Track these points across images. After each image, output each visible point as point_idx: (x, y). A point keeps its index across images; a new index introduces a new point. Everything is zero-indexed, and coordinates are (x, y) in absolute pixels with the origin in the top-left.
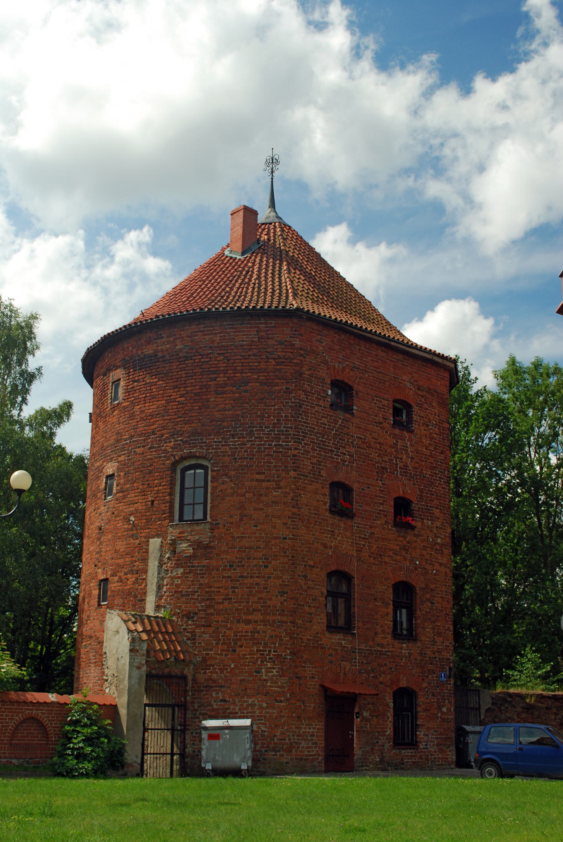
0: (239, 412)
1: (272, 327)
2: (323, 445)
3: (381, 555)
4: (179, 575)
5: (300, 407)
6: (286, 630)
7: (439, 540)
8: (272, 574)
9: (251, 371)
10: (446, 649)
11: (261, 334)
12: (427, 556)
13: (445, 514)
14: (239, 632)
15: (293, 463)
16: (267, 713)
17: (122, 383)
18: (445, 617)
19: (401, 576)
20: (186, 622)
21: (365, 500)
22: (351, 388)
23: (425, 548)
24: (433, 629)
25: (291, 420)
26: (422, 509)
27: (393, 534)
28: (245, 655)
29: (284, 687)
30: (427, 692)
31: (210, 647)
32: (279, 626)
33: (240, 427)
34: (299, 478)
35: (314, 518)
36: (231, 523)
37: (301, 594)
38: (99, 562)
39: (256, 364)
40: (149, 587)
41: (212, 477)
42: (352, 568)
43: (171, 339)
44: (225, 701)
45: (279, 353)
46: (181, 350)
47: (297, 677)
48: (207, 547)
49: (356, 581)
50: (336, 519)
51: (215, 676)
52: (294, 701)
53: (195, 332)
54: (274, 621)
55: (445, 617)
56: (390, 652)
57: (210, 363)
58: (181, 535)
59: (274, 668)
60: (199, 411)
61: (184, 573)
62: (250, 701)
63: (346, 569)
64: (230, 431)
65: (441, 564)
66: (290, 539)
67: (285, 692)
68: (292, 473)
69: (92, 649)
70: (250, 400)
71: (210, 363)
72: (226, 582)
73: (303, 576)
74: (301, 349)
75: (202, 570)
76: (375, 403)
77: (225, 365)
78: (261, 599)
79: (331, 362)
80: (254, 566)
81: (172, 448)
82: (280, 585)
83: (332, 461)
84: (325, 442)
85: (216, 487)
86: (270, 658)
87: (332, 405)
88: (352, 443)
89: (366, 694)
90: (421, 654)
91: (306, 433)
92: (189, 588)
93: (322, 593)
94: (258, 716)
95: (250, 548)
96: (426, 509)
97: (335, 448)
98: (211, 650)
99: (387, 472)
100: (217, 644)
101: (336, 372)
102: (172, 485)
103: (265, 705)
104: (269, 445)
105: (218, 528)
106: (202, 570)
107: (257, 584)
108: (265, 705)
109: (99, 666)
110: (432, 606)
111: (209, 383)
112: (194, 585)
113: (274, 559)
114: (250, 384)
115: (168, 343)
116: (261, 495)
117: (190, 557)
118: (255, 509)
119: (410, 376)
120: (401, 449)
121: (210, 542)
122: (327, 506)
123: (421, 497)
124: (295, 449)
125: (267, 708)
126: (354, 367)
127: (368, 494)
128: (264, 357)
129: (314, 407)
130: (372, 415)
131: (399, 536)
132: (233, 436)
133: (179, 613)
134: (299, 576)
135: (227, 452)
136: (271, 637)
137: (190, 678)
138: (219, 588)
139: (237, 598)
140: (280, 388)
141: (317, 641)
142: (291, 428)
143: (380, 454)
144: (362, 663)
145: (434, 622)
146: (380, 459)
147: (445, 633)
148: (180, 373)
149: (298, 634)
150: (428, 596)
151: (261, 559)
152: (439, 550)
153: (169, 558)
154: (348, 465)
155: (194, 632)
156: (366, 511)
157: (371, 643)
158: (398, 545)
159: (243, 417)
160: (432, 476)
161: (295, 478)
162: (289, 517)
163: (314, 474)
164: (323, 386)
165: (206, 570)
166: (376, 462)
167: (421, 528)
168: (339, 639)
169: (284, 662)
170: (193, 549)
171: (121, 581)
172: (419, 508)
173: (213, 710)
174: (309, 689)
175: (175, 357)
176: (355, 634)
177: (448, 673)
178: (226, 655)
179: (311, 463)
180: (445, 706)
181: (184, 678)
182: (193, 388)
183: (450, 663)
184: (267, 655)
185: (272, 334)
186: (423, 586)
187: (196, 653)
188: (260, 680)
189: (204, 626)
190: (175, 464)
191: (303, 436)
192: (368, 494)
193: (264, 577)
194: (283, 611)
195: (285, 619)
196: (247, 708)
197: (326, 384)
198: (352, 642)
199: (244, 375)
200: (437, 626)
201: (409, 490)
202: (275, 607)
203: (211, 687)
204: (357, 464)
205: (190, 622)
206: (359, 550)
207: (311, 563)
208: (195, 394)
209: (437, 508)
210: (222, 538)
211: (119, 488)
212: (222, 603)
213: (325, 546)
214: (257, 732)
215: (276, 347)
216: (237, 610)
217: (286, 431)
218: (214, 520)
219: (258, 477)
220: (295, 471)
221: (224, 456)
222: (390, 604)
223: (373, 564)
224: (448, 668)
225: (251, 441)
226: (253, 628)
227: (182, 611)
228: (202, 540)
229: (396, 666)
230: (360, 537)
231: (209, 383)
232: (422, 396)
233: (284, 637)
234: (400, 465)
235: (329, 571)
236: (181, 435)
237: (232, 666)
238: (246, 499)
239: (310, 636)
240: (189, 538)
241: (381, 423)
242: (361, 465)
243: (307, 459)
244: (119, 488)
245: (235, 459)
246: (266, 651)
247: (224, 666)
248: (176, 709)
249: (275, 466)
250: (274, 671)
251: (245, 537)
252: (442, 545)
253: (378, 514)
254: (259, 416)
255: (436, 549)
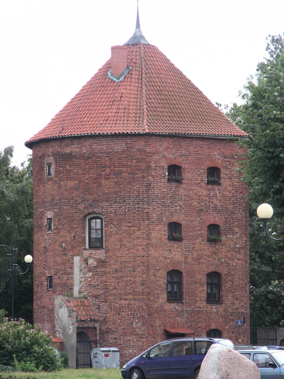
0: (118, 190)
1: (134, 141)
2: (164, 204)
3: (199, 259)
4: (90, 276)
5: (150, 185)
6: (145, 303)
7: (238, 246)
8: (137, 275)
9: (123, 167)
10: (242, 307)
11: (128, 145)
12: (230, 256)
13: (242, 229)
14: (122, 305)
15: (147, 216)
16: (137, 344)
17: (53, 166)
18: (242, 289)
19: (212, 269)
20: (95, 300)
21: (189, 230)
22: (180, 167)
23: (228, 251)
24: (233, 296)
25: (145, 193)
26: (227, 229)
27: (207, 246)
28: (125, 316)
29: (145, 331)
30: (228, 331)
31: (107, 312)
32: (141, 301)
33: (118, 198)
34: (150, 224)
35: (159, 244)
36: (116, 249)
37: (153, 284)
38: (46, 266)
39: (126, 163)
40: (75, 282)
41: (105, 225)
42: (182, 268)
43: (80, 146)
44: (116, 339)
45: (138, 156)
46: (85, 153)
47: (151, 326)
48: (104, 262)
49: (184, 275)
50: (172, 243)
51: (110, 327)
52: (150, 338)
53: (92, 143)
54: (139, 299)
55: (242, 289)
56: (205, 311)
57: (102, 161)
58: (90, 255)
59: (140, 322)
60: (96, 188)
61: (92, 275)
62: (128, 338)
63: (178, 269)
64: (113, 200)
65: (239, 259)
66: (146, 256)
67: (145, 334)
68: (146, 222)
69: (46, 313)
70: (123, 183)
71: (102, 161)
72: (114, 279)
73: (154, 275)
74: (150, 153)
75: (102, 274)
76: (196, 173)
77: (110, 163)
78: (132, 288)
79: (168, 155)
80: (128, 271)
81: (83, 208)
82: (142, 280)
83: (169, 212)
84: (165, 202)
85: (107, 230)
86: (137, 317)
87: (168, 181)
88: (181, 199)
89: (189, 334)
90: (225, 311)
91: (154, 199)
92: (96, 283)
93: (164, 283)
94: (132, 346)
95: (126, 262)
96: (229, 229)
97: (171, 204)
98: (108, 314)
99: (203, 211)
100: (111, 311)
101: (171, 161)
102: (84, 228)
103: (135, 340)
104: (134, 207)
105: (109, 252)
106: (102, 274)
107: (130, 280)
108: (135, 340)
109: (50, 322)
110: (233, 284)
111: (101, 173)
112: (98, 281)
113: (138, 268)
114: (123, 174)
115: (78, 148)
116: (131, 234)
117: (95, 267)
118: (127, 242)
119: (219, 151)
120: (212, 196)
121: (105, 259)
122: (167, 237)
123: (226, 222)
124: (148, 209)
125: (137, 341)
126: (182, 155)
127: (191, 226)
128: (130, 158)
129: (158, 184)
130: (193, 180)
131: (211, 247)
132: (115, 202)
133: (91, 296)
134: (151, 275)
135: (112, 211)
136: (138, 307)
137: (98, 328)
138: (111, 282)
139: (120, 288)
140: (139, 175)
141: (162, 308)
142: (145, 197)
143: (198, 202)
144: (188, 317)
145: (234, 293)
146: (199, 205)
147: (241, 298)
148: (85, 166)
149: (151, 305)
150: (230, 278)
151: (131, 267)
152: (237, 251)
153: (84, 267)
154: (178, 212)
155: (99, 305)
156: (190, 236)
157: (193, 307)
158: (210, 252)
159: (120, 192)
160: (233, 208)
161: (148, 224)
162: (145, 245)
163: (158, 221)
164: (163, 171)
165: (104, 274)
166: (196, 207)
167: (225, 241)
168: (174, 306)
169: (145, 319)
170: (97, 263)
171: (60, 278)
172: (224, 229)
173: (110, 343)
174: (158, 332)
175: (82, 157)
176: (183, 302)
177: (243, 320)
178: (115, 316)
179: (157, 215)
180: (240, 338)
181: (95, 328)
182: (92, 175)
183: (244, 315)
184: (136, 316)
185: (134, 145)
186: (226, 273)
187: (100, 315)
188: (133, 328)
189: (104, 302)
190: (85, 216)
191: (152, 201)
192: (191, 226)
193: (133, 277)
194: (143, 293)
195: (144, 297)
196: (127, 342)
197: (165, 169)
198: (182, 307)
199: (120, 169)
200: (236, 295)
201: (217, 219)
202: (139, 291)
203: (109, 332)
204: (185, 210)
205: (97, 300)
206: (186, 258)
207: (158, 268)
208: (94, 179)
209: (236, 227)
210: (111, 257)
211: (55, 227)
212: (113, 290)
213: (166, 258)
214: (132, 353)
215: (136, 152)
216: (120, 293)
217: (143, 199)
218: (107, 248)
219: (129, 224)
220: (148, 220)
221: (110, 213)
222: (205, 285)
223: (195, 264)
224: (243, 318)
225: (124, 205)
226: (129, 303)
227: (93, 295)
228: (101, 258)
229: (209, 318)
230: (186, 251)
231: (101, 173)
232: (227, 161)
233: (144, 306)
234: (212, 205)
235: (168, 271)
236: (88, 201)
237: (119, 322)
238: (123, 236)
239: (158, 305)
240: (94, 257)
241: (200, 184)
242: (187, 210)
243: (155, 213)
244: (55, 227)
245: (116, 215)
246: (135, 314)
247: (115, 322)
248: (92, 343)
249: (137, 219)
250: (140, 323)
251: (123, 257)
252: (240, 248)
253: (197, 236)
254: (128, 192)
255: (236, 251)
